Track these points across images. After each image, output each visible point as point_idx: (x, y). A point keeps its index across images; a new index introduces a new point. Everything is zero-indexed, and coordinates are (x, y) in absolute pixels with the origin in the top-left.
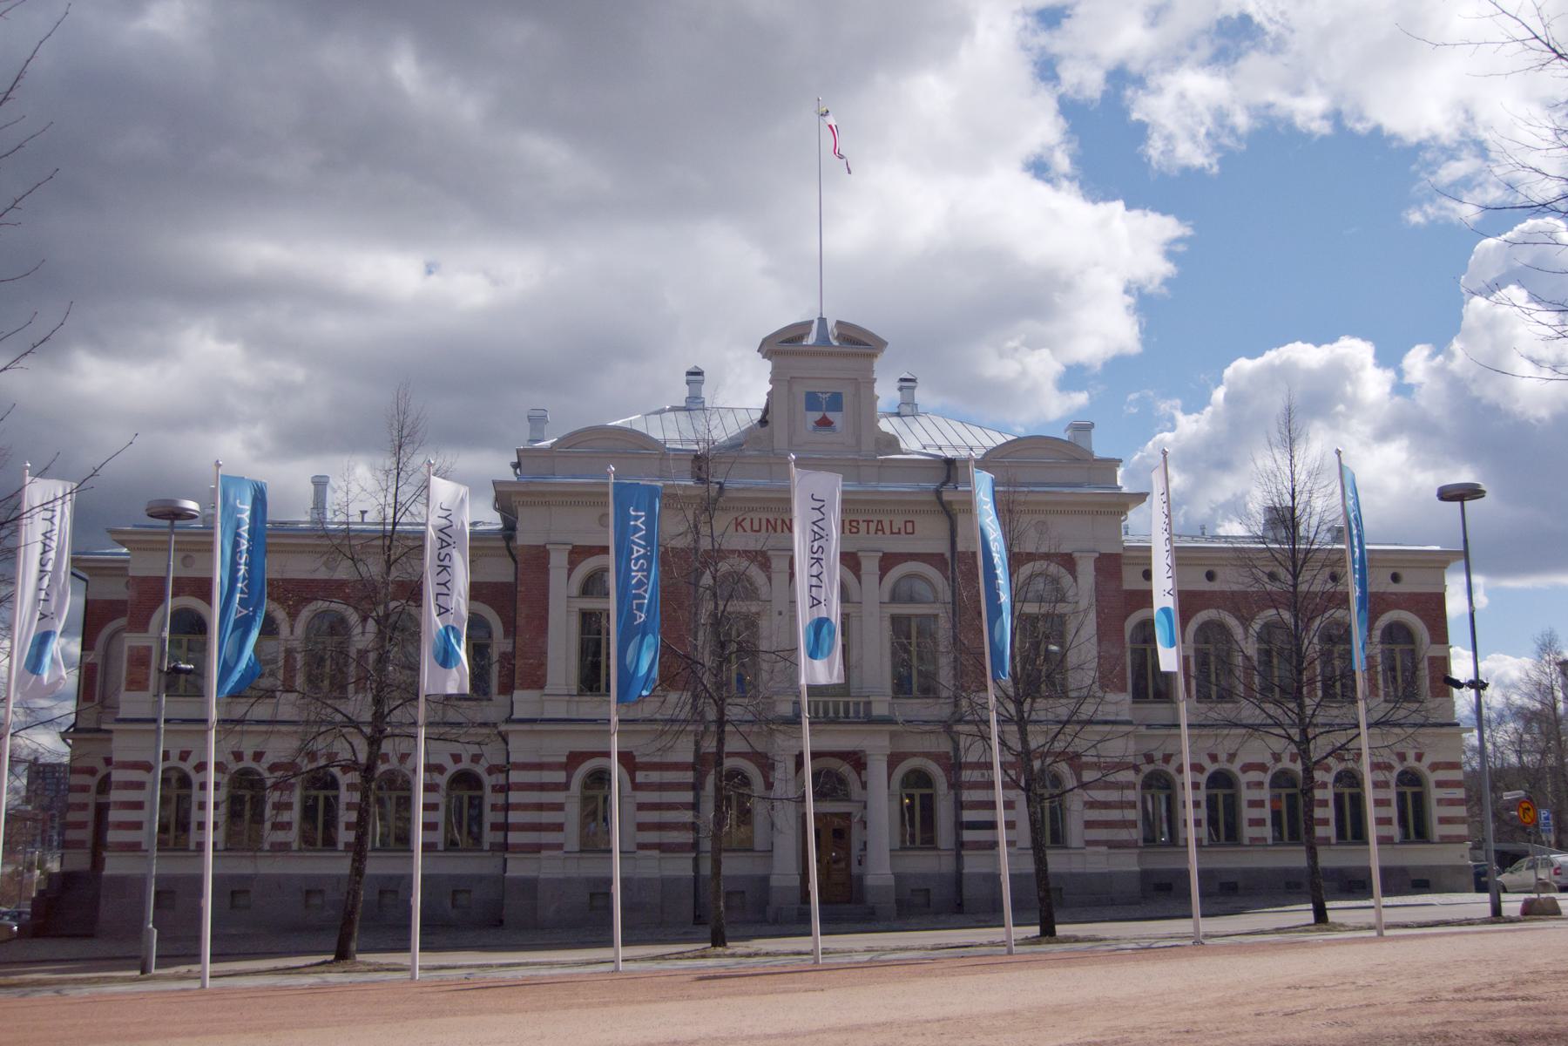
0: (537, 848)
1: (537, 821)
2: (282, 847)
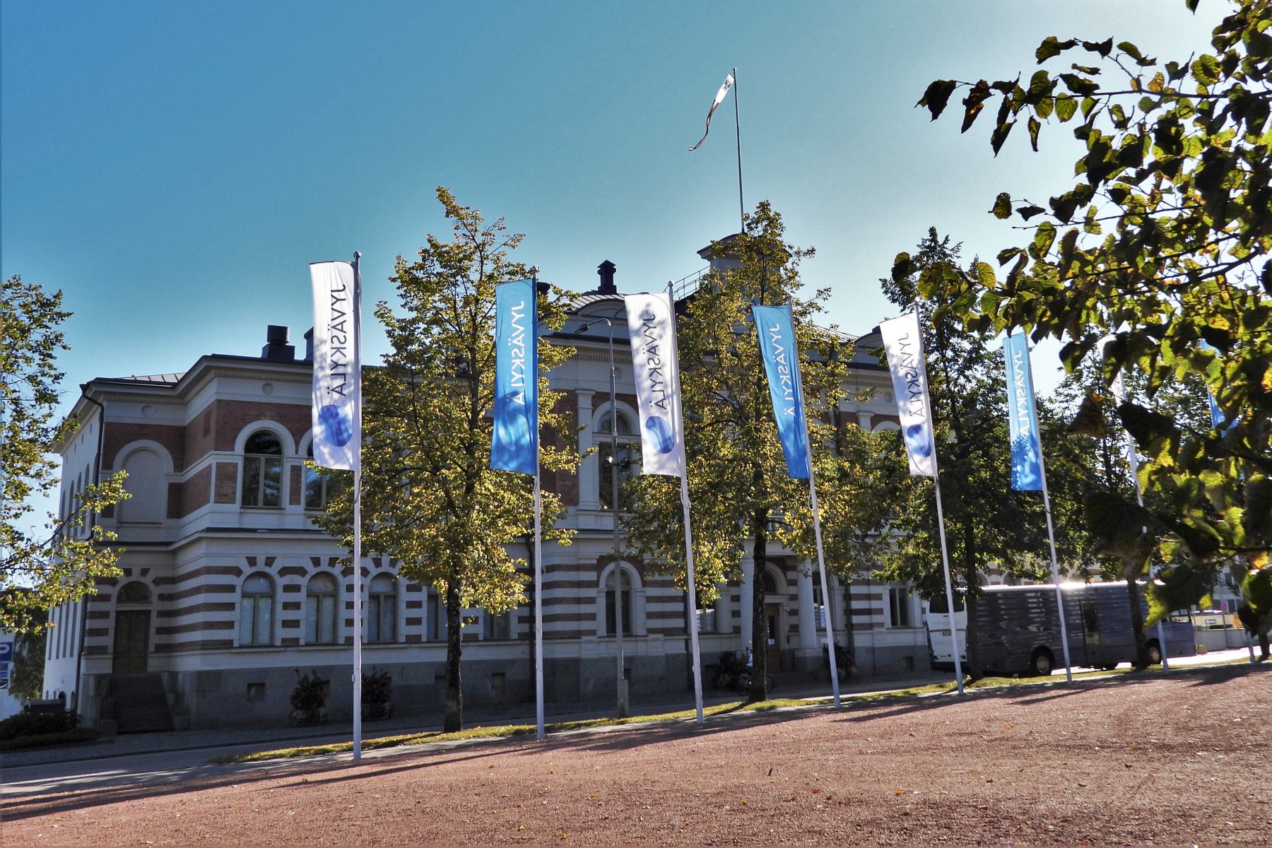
0: (577, 635)
1: (167, 625)
2: (413, 640)
